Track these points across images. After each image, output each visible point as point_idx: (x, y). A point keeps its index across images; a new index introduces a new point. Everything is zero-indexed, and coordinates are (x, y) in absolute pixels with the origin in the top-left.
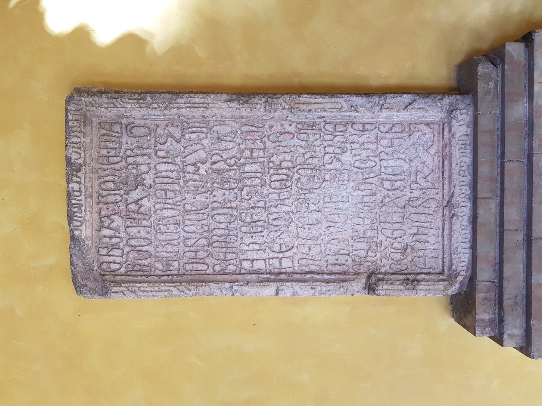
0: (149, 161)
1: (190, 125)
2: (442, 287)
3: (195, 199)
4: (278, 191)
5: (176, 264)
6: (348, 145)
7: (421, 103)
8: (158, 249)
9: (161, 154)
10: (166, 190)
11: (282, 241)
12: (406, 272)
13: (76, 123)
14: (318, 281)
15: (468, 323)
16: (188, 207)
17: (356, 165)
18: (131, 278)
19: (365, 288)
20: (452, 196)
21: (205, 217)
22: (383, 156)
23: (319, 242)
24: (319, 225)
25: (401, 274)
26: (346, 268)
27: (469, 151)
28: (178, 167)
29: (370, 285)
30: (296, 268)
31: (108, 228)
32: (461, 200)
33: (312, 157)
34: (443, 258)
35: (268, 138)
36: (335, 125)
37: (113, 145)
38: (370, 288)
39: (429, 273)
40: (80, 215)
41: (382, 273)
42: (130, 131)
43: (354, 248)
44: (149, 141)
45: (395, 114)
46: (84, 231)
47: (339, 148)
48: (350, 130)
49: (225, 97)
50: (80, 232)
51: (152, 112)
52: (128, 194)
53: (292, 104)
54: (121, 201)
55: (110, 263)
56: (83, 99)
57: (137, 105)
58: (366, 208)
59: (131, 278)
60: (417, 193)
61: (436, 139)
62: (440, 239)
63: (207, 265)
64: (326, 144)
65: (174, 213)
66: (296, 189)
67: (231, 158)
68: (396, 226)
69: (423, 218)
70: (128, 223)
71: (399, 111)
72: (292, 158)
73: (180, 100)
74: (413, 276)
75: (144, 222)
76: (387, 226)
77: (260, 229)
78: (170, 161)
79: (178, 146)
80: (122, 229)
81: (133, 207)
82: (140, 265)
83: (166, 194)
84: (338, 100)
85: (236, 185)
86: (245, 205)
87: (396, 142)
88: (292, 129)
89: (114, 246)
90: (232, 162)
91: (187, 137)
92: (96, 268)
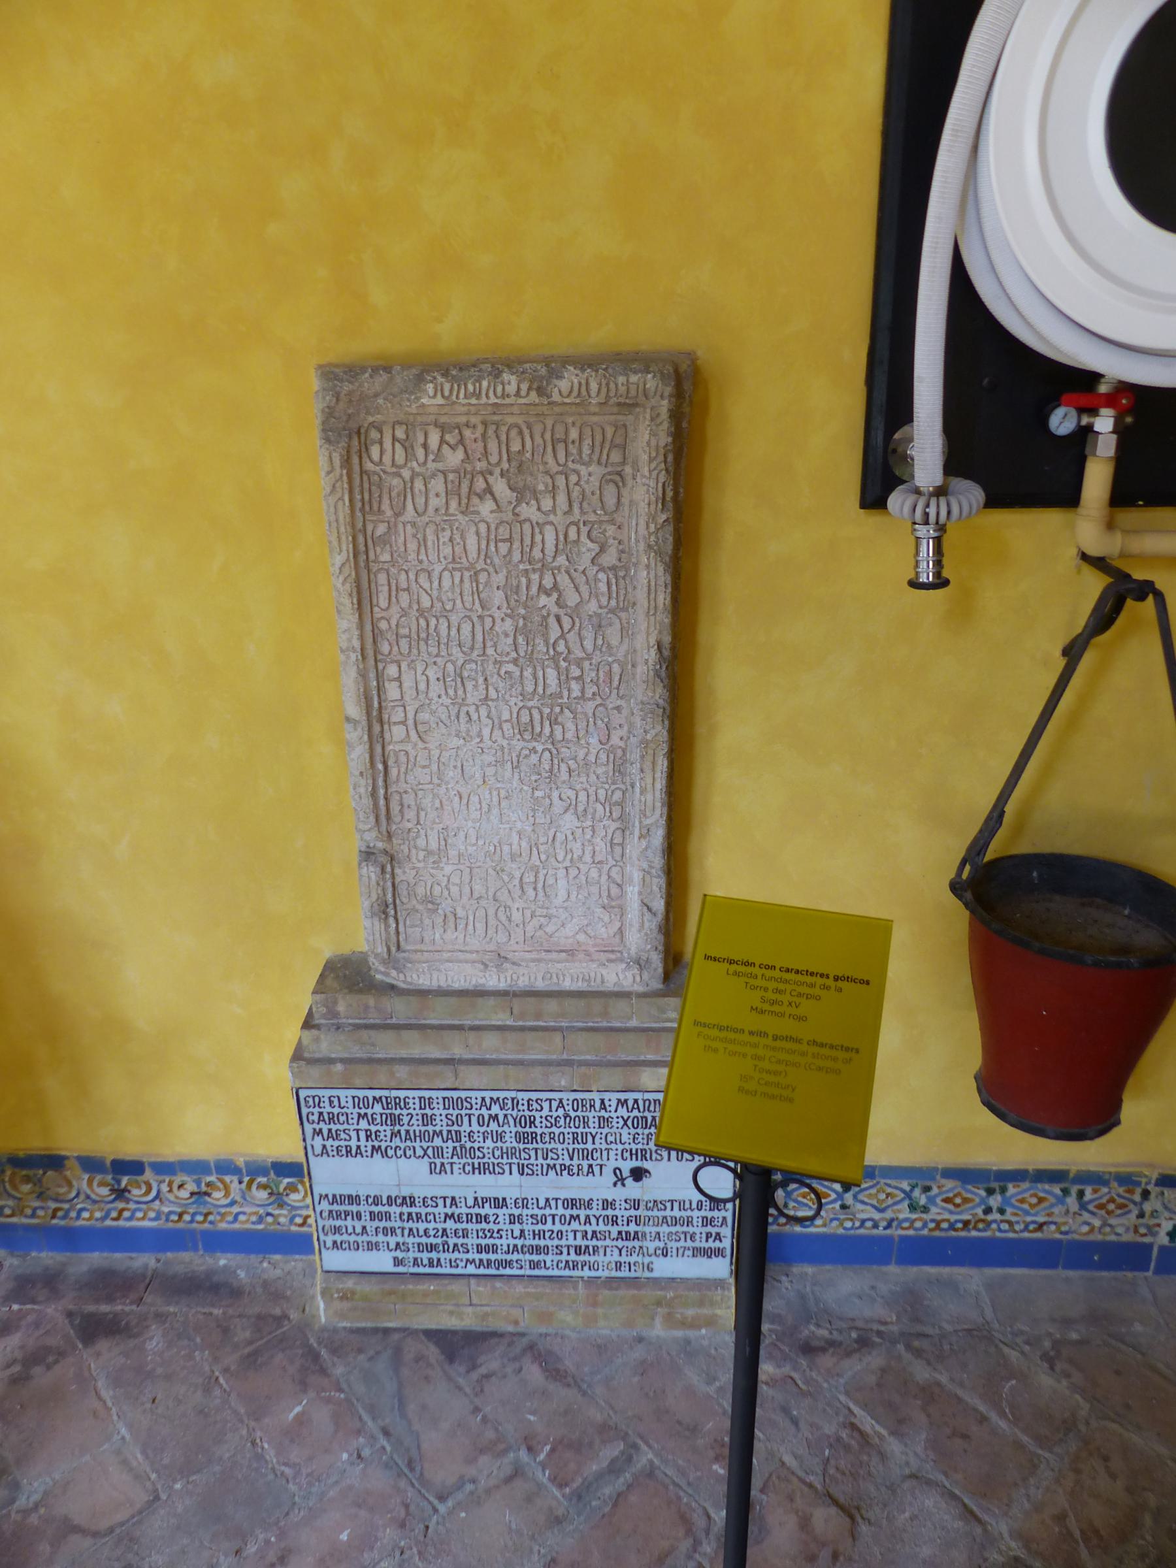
0: (559, 512)
1: (621, 581)
2: (379, 950)
3: (498, 588)
4: (514, 720)
5: (386, 557)
6: (589, 823)
7: (652, 924)
8: (409, 527)
9: (572, 534)
10: (510, 540)
11: (434, 726)
12: (398, 901)
13: (622, 389)
14: (374, 781)
15: (329, 981)
16: (483, 577)
17: (558, 834)
18: (357, 482)
19: (368, 847)
20: (514, 963)
21: (468, 605)
22: (573, 872)
23: (436, 781)
24: (462, 782)
25: (394, 895)
26: (397, 819)
27: (581, 986)
28: (550, 560)
29: (373, 853)
30: (391, 747)
31: (442, 441)
32: (508, 975)
33: (570, 771)
34: (422, 951)
35: (600, 705)
36: (621, 804)
37: (586, 451)
38: (368, 855)
39: (398, 933)
40: (462, 395)
41: (393, 870)
42: (611, 480)
43: (429, 832)
44: (595, 512)
45: (636, 889)
46: (434, 401)
47: (585, 810)
48: (614, 825)
49: (667, 639)
50: (431, 394)
51: (642, 523)
52: (502, 475)
53: (653, 746)
54: (489, 463)
55: (381, 443)
56: (665, 402)
57: (653, 498)
58: (492, 848)
59: (357, 482)
60: (517, 916)
61: (599, 941)
62: (450, 947)
63: (388, 608)
64: (592, 791)
65: (473, 554)
66: (518, 748)
67: (567, 647)
68: (467, 890)
69: (480, 926)
70: (451, 476)
71: (640, 893)
72: (568, 741)
73: (661, 569)
74: (392, 912)
75: (454, 504)
76: (466, 878)
77: (451, 692)
78: (561, 547)
79: (585, 561)
80: (440, 466)
81: (480, 484)
82: (380, 496)
83: (503, 541)
84: (658, 812)
85: (522, 654)
86: (491, 667)
87: (594, 889)
88: (615, 740)
89: (410, 450)
90: (561, 647)
91: (601, 576)
92: (371, 419)
